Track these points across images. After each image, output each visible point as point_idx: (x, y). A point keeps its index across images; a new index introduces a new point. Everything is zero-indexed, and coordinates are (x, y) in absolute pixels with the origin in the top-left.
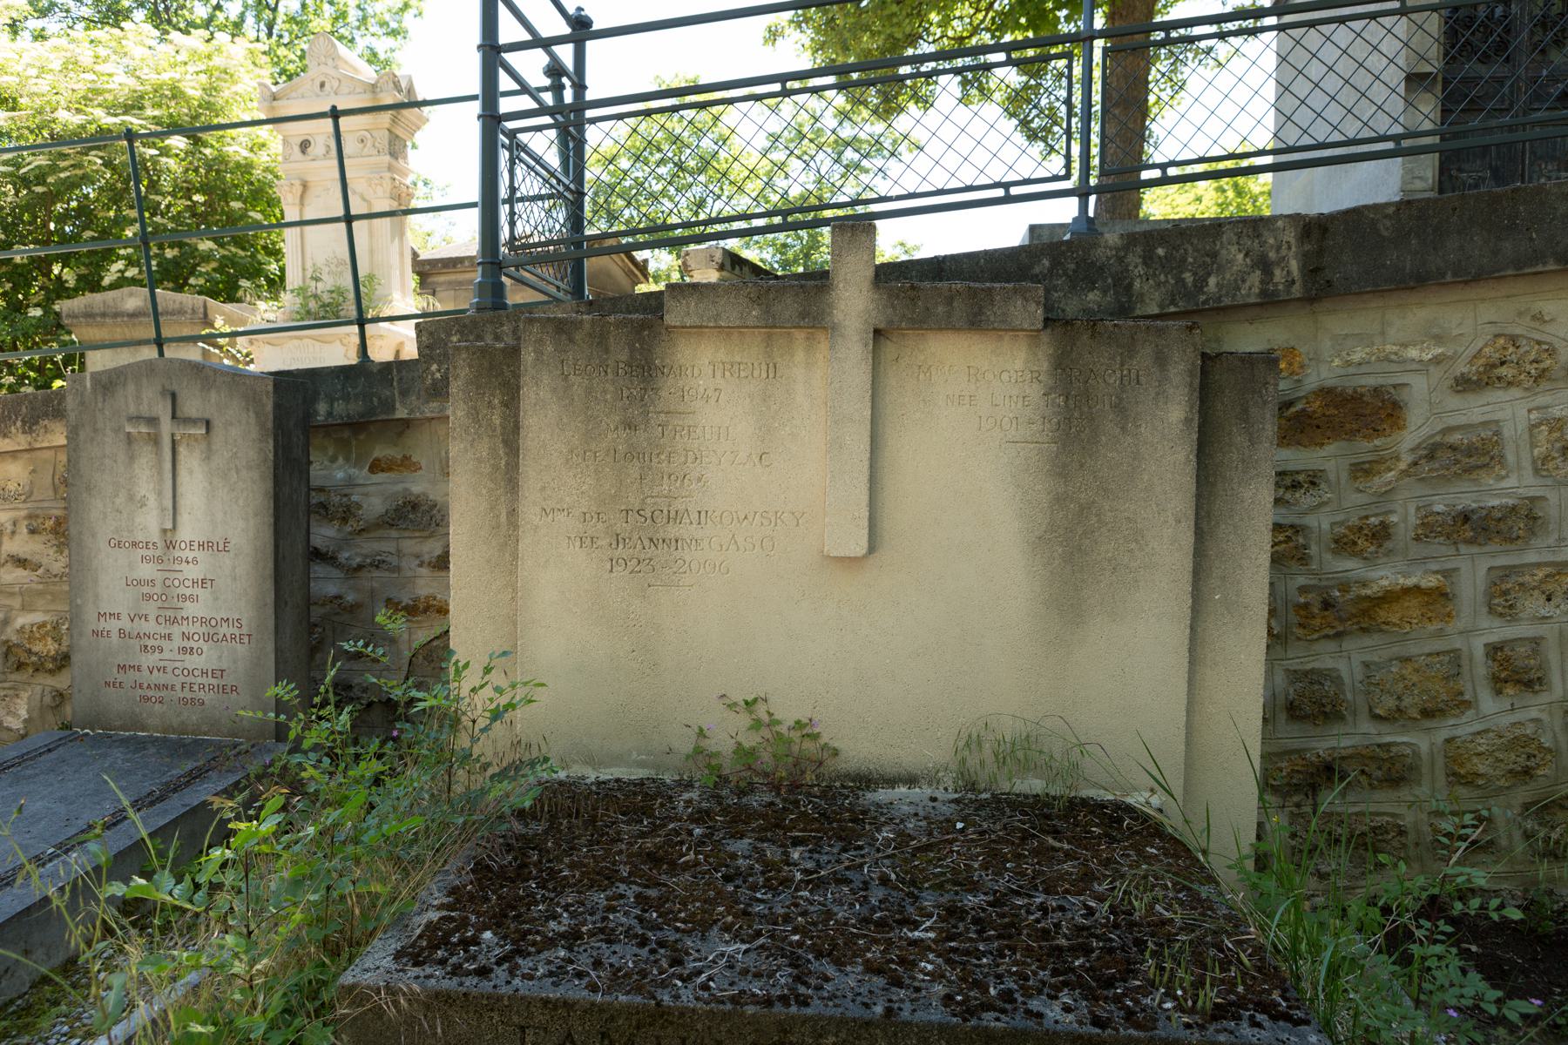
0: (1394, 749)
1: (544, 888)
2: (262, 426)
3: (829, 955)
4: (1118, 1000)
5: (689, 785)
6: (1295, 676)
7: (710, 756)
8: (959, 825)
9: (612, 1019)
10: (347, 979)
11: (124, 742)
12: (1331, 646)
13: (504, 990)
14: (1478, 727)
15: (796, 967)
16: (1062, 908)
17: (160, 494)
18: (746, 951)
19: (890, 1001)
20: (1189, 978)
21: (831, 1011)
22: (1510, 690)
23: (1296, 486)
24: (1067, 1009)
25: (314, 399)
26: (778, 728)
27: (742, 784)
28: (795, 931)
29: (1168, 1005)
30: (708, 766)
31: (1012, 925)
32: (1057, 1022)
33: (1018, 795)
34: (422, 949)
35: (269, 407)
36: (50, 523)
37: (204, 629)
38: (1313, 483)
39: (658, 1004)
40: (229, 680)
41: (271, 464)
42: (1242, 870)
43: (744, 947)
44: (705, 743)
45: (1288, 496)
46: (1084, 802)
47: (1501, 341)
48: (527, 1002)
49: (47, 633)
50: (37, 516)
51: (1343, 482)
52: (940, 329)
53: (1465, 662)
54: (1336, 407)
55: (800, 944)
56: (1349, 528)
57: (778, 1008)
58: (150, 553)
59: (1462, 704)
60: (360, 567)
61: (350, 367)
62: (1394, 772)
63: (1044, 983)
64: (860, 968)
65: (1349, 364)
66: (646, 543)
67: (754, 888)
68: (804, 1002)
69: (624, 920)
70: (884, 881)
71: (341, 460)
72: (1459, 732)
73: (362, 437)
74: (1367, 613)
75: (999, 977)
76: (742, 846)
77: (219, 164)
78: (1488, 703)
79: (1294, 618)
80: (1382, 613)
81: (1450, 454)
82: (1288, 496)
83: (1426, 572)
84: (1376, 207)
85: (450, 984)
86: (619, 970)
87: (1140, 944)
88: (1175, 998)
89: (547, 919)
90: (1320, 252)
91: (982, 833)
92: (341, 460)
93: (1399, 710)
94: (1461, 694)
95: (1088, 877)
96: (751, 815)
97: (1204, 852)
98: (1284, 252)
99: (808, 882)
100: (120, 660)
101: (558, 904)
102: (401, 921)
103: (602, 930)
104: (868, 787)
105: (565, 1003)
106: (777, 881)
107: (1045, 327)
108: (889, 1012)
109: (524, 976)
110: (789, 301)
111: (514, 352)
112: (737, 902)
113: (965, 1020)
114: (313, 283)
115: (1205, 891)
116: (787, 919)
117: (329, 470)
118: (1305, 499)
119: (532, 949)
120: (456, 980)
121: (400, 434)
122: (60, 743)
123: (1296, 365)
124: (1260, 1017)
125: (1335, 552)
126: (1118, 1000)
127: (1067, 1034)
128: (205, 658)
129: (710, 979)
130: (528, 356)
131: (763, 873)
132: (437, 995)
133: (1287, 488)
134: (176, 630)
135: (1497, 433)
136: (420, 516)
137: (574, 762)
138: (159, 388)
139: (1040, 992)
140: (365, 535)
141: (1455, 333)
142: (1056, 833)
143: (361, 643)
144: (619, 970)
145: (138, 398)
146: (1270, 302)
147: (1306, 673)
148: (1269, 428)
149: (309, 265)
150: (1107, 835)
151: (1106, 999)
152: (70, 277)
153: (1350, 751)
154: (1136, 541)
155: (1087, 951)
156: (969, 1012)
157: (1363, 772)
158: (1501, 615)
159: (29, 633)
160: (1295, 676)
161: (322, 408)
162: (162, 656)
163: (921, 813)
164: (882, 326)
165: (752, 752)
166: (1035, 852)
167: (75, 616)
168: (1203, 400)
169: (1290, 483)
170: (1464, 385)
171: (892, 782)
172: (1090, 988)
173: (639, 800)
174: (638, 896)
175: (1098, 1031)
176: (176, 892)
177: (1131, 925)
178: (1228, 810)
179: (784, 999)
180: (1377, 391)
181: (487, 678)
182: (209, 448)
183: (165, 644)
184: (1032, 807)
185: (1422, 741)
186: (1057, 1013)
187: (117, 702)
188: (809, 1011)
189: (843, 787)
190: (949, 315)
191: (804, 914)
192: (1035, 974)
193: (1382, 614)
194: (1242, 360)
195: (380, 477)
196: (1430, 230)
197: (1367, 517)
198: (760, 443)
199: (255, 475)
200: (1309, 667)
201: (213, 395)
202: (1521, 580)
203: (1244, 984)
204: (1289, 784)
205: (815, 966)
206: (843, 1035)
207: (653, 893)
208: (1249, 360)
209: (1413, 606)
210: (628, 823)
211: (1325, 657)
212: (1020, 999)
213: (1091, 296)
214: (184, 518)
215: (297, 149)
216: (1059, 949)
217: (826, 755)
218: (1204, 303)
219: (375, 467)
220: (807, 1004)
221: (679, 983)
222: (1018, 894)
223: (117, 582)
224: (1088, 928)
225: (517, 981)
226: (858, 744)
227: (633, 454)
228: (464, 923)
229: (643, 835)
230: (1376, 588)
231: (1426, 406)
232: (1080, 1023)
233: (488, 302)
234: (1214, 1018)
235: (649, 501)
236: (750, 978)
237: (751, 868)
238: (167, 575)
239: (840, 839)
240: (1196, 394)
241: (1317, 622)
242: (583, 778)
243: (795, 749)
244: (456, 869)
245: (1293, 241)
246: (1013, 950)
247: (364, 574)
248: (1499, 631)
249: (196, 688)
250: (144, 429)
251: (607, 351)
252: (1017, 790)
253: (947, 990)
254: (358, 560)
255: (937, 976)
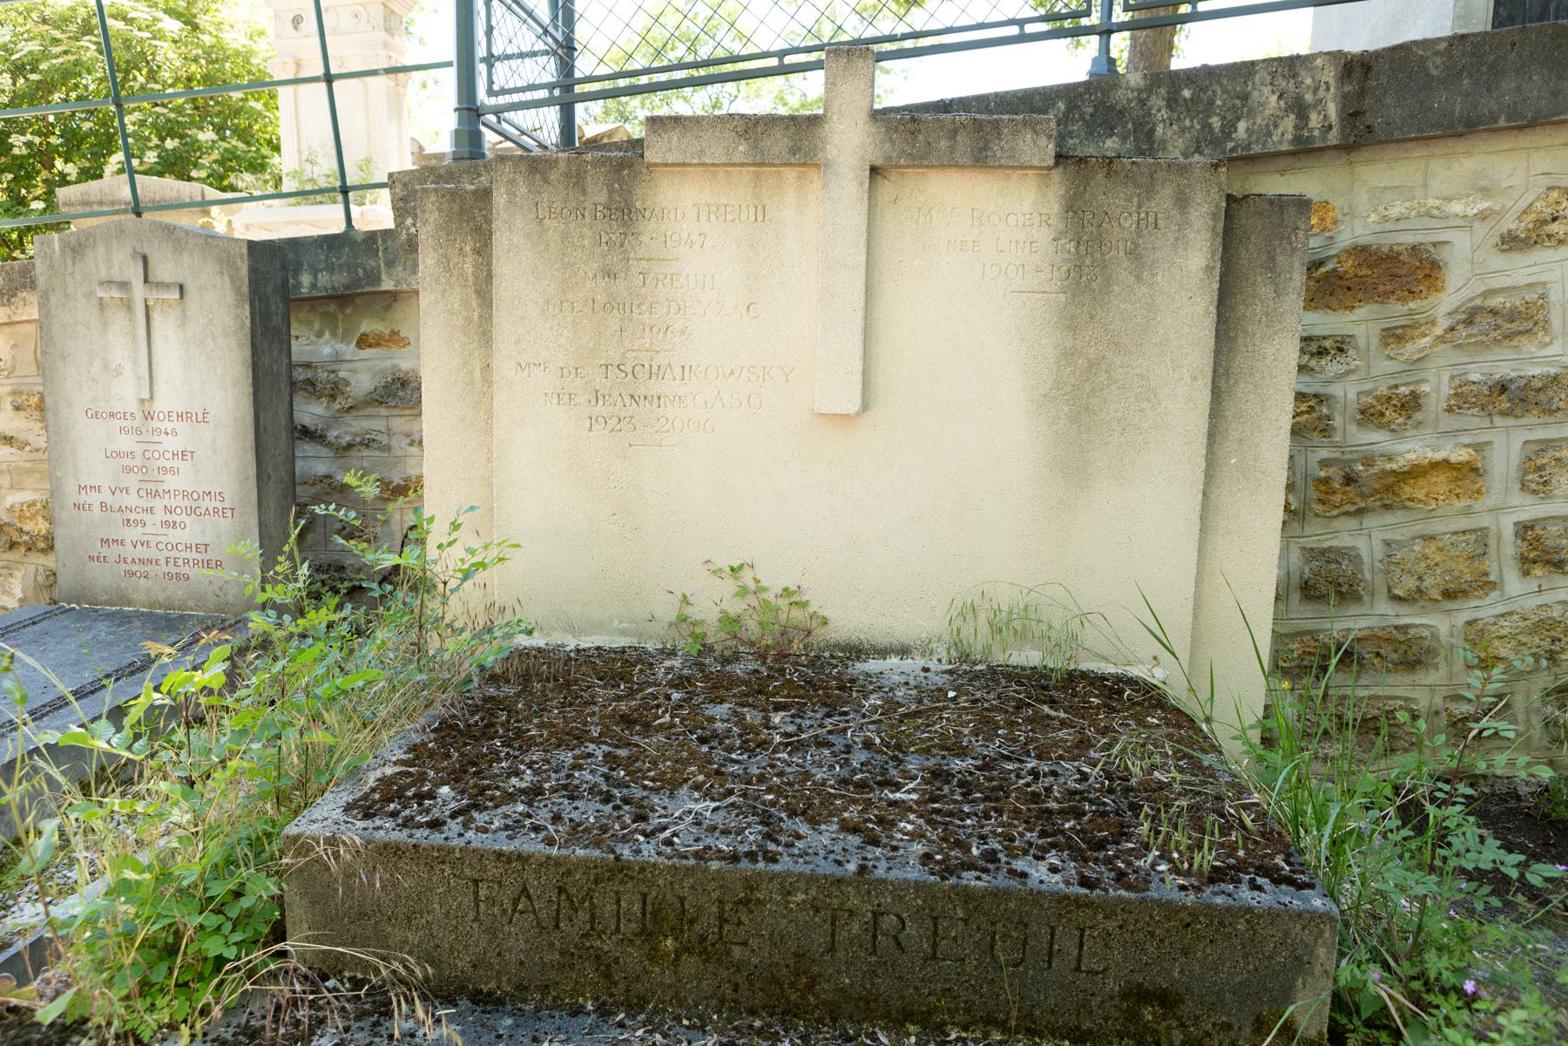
0: (1412, 631)
1: (509, 746)
2: (238, 291)
3: (804, 813)
4: (1109, 861)
5: (672, 654)
6: (1311, 554)
7: (694, 624)
8: (951, 694)
9: (569, 873)
10: (292, 830)
11: (110, 616)
12: (1352, 523)
13: (457, 842)
14: (1501, 609)
15: (767, 825)
16: (1054, 774)
17: (135, 362)
18: (714, 810)
19: (865, 859)
20: (1185, 842)
21: (801, 867)
22: (1538, 571)
23: (1322, 352)
24: (1054, 870)
25: (297, 271)
26: (764, 596)
27: (727, 653)
28: (769, 790)
29: (1163, 868)
30: (692, 634)
31: (1001, 788)
32: (1042, 882)
33: (1015, 667)
34: (375, 802)
35: (244, 271)
36: (35, 400)
37: (187, 503)
38: (1341, 350)
39: (617, 859)
40: (213, 555)
41: (248, 331)
42: (1247, 742)
43: (714, 805)
44: (688, 611)
45: (1313, 363)
46: (1084, 675)
47: (1555, 194)
48: (481, 855)
49: (37, 512)
50: (21, 393)
51: (1373, 348)
52: (942, 166)
53: (1492, 542)
54: (1369, 267)
55: (773, 804)
56: (1377, 398)
57: (745, 864)
58: (128, 424)
59: (1486, 585)
60: (350, 446)
61: (334, 237)
62: (1411, 655)
63: (1030, 844)
64: (835, 827)
65: (1385, 219)
66: (627, 400)
67: (730, 749)
68: (772, 858)
69: (589, 777)
70: (868, 744)
71: (327, 335)
72: (1480, 614)
73: (348, 311)
74: (1392, 489)
75: (983, 838)
76: (721, 710)
77: (215, 55)
78: (1514, 584)
79: (1313, 494)
80: (1407, 489)
81: (1490, 319)
82: (1313, 363)
83: (1456, 445)
84: (1425, 43)
85: (400, 836)
86: (579, 825)
87: (1135, 808)
88: (1171, 861)
89: (509, 776)
90: (1362, 93)
91: (975, 701)
92: (327, 335)
93: (1419, 590)
94: (1487, 574)
95: (1084, 744)
96: (734, 681)
97: (1208, 720)
98: (1321, 93)
99: (787, 745)
100: (103, 534)
101: (522, 762)
102: (354, 773)
103: (565, 787)
104: (858, 658)
105: (520, 856)
106: (754, 743)
107: (1057, 164)
108: (862, 869)
109: (478, 829)
110: (778, 135)
111: (485, 195)
112: (710, 763)
113: (943, 878)
114: (308, 167)
115: (1208, 760)
116: (762, 779)
117: (312, 344)
118: (1331, 367)
119: (490, 804)
120: (406, 832)
121: (388, 308)
122: (46, 616)
123: (1329, 220)
124: (1260, 881)
125: (1359, 424)
126: (1109, 861)
127: (1052, 894)
128: (190, 532)
129: (675, 834)
130: (500, 198)
131: (740, 736)
132: (386, 846)
133: (1312, 355)
134: (158, 504)
135: (1542, 297)
136: (400, 392)
137: (554, 629)
138: (130, 251)
139: (1025, 852)
140: (354, 413)
141: (1505, 185)
142: (1052, 703)
143: (333, 506)
144: (579, 825)
145: (108, 260)
146: (1304, 151)
147: (1323, 552)
148: (1297, 279)
149: (304, 147)
150: (1105, 705)
151: (1096, 860)
152: (71, 170)
153: (1365, 633)
154: (1149, 400)
155: (1079, 814)
156: (948, 870)
157: (1378, 654)
158: (1534, 492)
159: (23, 512)
160: (1311, 554)
161: (306, 279)
162: (145, 530)
163: (912, 683)
164: (879, 162)
165: (736, 620)
166: (1029, 720)
167: (55, 492)
168: (1225, 248)
169: (1315, 348)
170: (1511, 243)
171: (883, 653)
172: (1081, 850)
173: (619, 666)
174: (607, 755)
175: (1086, 891)
176: (114, 741)
177: (1128, 790)
178: (1236, 691)
179: (751, 856)
180: (1415, 249)
181: (455, 535)
182: (184, 316)
183: (147, 517)
184: (1029, 678)
185: (1442, 624)
186: (1045, 874)
187: (102, 577)
188: (777, 868)
189: (832, 657)
190: (952, 150)
191: (780, 774)
192: (1021, 835)
193: (1407, 491)
194: (1271, 202)
195: (368, 353)
196: (1484, 69)
197: (1396, 387)
198: (742, 282)
199: (232, 342)
200: (1326, 545)
201: (186, 258)
202: (1558, 455)
203: (1245, 847)
204: (1299, 666)
205: (788, 824)
206: (813, 892)
207: (623, 753)
208: (1279, 203)
209: (1441, 481)
210: (604, 687)
211: (1344, 535)
212: (1004, 859)
213: (1109, 143)
214: (160, 387)
215: (289, 25)
216: (1049, 811)
217: (814, 624)
218: (1232, 150)
219: (363, 342)
220: (775, 861)
221: (641, 838)
222: (1008, 758)
223: (95, 457)
224: (1081, 793)
225: (470, 834)
226: (847, 613)
227: (611, 305)
228: (422, 778)
229: (618, 698)
230: (1402, 462)
231: (1468, 266)
232: (1067, 883)
233: (466, 150)
234: (1212, 881)
235: (630, 355)
236: (717, 834)
237: (729, 730)
238: (147, 446)
239: (825, 705)
240: (1219, 239)
241: (1338, 498)
242: (563, 646)
243: (783, 617)
244: (415, 730)
245: (1332, 82)
246: (1000, 812)
247: (354, 453)
248: (1530, 509)
249: (180, 562)
250: (116, 294)
251: (584, 192)
252: (1014, 661)
253: (926, 849)
254: (348, 438)
255: (917, 836)
